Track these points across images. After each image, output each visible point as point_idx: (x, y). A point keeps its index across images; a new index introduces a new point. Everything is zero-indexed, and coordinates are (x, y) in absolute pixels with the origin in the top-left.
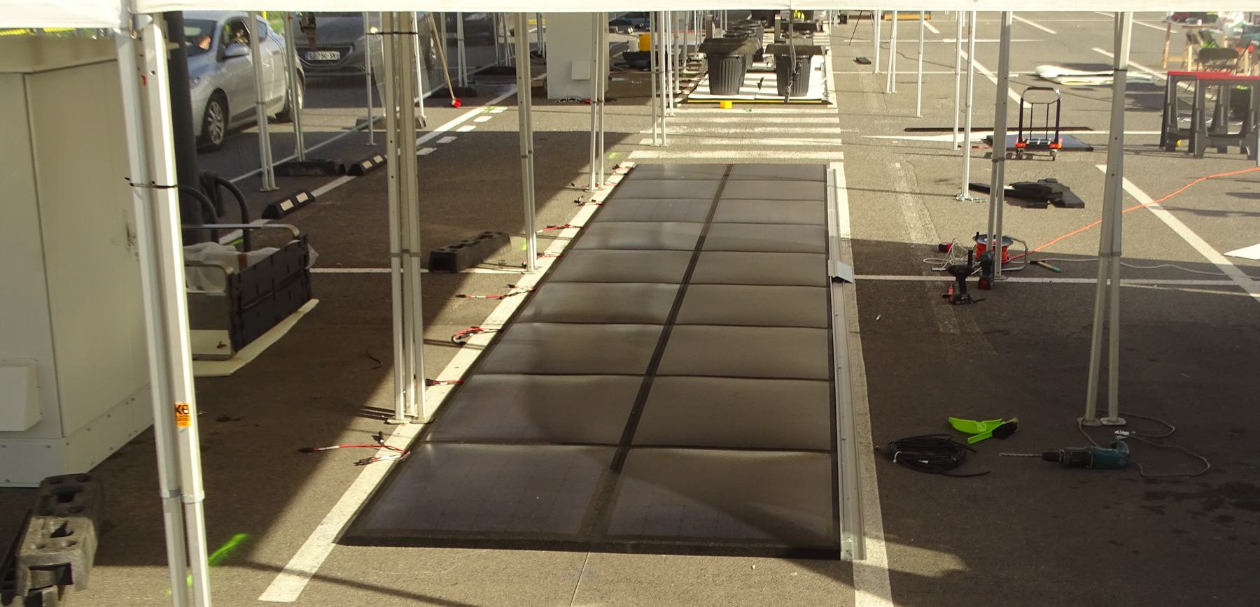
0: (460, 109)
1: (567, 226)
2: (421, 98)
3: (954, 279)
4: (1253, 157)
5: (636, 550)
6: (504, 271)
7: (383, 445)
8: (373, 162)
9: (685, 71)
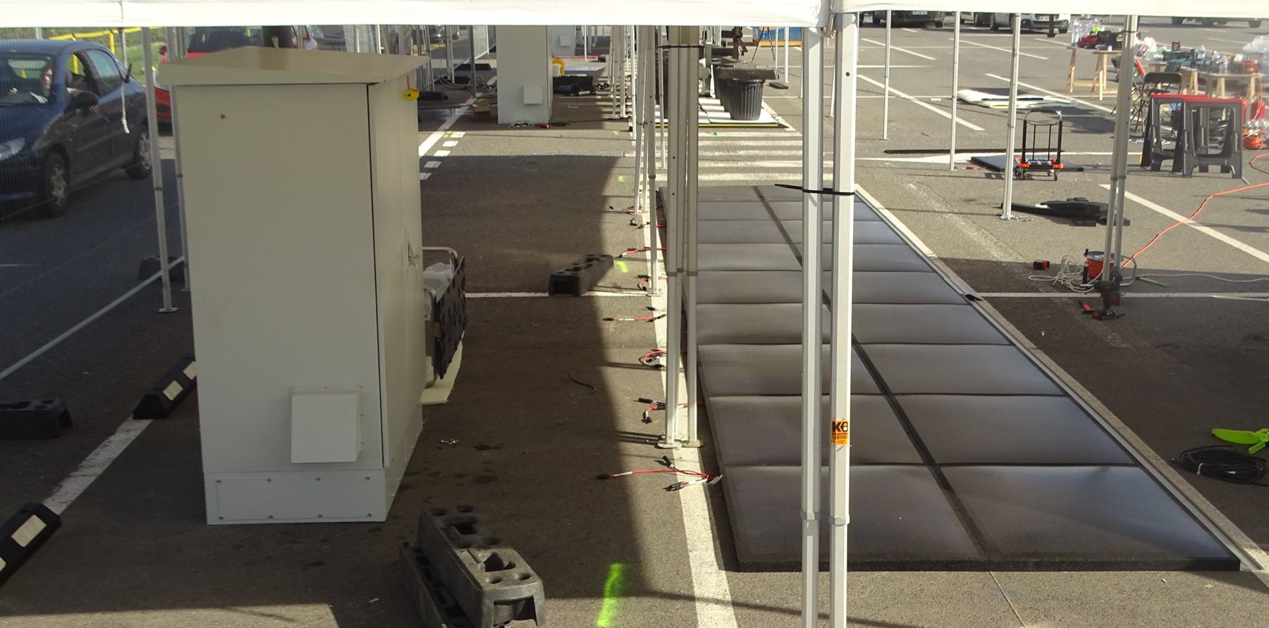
3: (1098, 295)
4: (1238, 175)
5: (1038, 567)
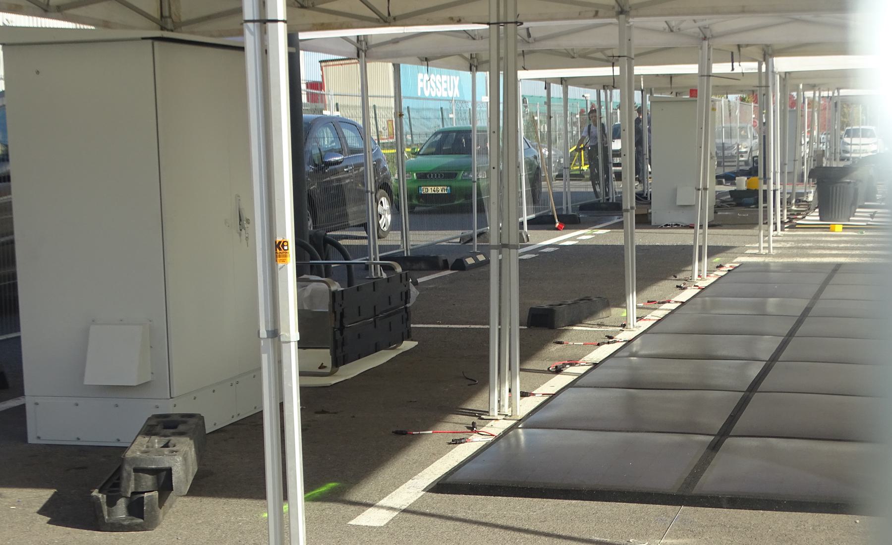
0: (565, 231)
1: (669, 302)
2: (525, 218)
6: (603, 329)
7: (476, 432)
8: (476, 259)
9: (794, 208)
